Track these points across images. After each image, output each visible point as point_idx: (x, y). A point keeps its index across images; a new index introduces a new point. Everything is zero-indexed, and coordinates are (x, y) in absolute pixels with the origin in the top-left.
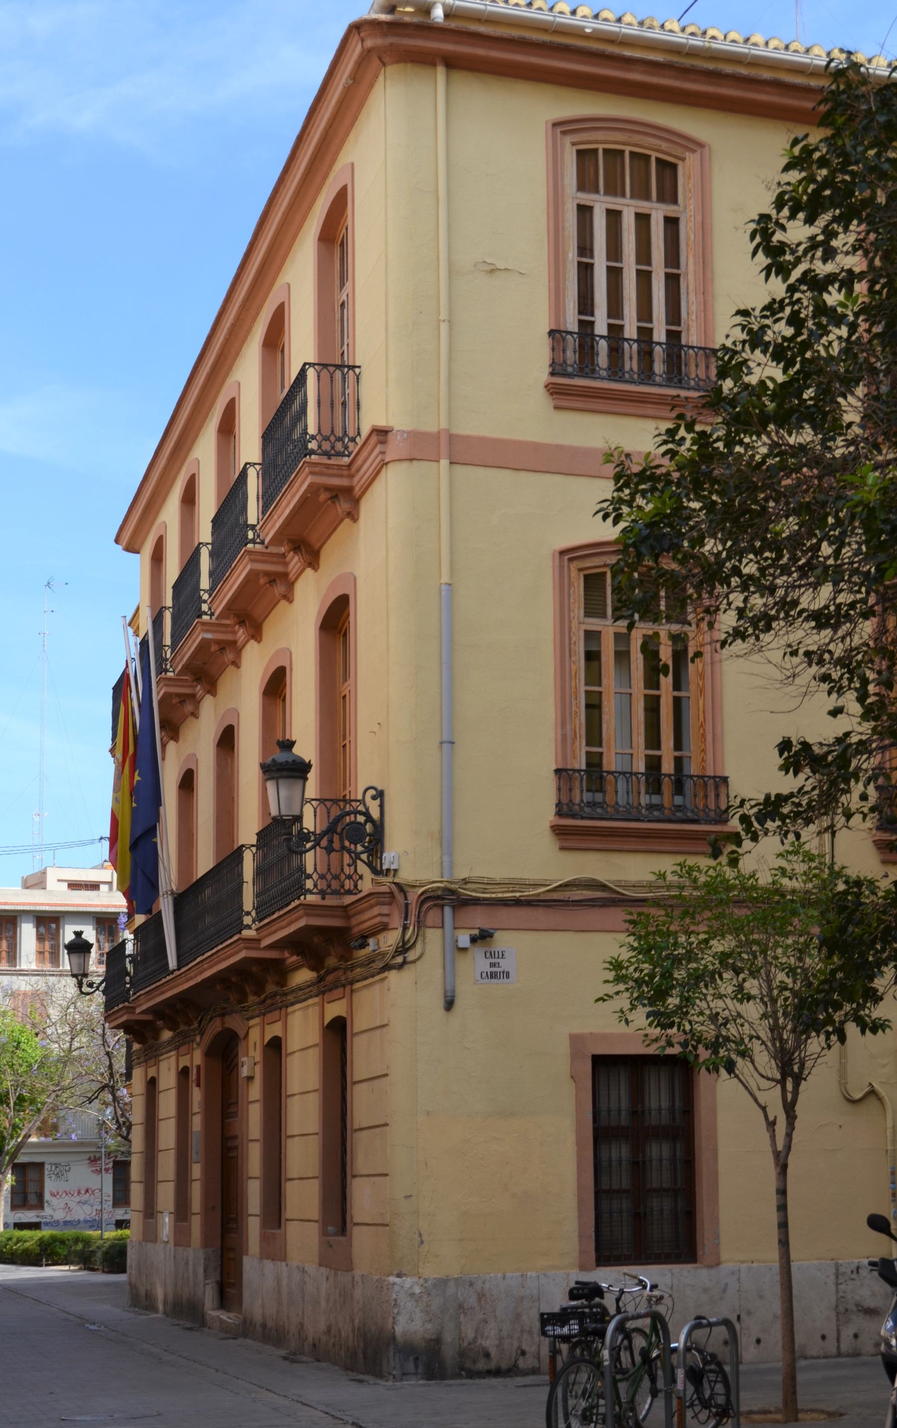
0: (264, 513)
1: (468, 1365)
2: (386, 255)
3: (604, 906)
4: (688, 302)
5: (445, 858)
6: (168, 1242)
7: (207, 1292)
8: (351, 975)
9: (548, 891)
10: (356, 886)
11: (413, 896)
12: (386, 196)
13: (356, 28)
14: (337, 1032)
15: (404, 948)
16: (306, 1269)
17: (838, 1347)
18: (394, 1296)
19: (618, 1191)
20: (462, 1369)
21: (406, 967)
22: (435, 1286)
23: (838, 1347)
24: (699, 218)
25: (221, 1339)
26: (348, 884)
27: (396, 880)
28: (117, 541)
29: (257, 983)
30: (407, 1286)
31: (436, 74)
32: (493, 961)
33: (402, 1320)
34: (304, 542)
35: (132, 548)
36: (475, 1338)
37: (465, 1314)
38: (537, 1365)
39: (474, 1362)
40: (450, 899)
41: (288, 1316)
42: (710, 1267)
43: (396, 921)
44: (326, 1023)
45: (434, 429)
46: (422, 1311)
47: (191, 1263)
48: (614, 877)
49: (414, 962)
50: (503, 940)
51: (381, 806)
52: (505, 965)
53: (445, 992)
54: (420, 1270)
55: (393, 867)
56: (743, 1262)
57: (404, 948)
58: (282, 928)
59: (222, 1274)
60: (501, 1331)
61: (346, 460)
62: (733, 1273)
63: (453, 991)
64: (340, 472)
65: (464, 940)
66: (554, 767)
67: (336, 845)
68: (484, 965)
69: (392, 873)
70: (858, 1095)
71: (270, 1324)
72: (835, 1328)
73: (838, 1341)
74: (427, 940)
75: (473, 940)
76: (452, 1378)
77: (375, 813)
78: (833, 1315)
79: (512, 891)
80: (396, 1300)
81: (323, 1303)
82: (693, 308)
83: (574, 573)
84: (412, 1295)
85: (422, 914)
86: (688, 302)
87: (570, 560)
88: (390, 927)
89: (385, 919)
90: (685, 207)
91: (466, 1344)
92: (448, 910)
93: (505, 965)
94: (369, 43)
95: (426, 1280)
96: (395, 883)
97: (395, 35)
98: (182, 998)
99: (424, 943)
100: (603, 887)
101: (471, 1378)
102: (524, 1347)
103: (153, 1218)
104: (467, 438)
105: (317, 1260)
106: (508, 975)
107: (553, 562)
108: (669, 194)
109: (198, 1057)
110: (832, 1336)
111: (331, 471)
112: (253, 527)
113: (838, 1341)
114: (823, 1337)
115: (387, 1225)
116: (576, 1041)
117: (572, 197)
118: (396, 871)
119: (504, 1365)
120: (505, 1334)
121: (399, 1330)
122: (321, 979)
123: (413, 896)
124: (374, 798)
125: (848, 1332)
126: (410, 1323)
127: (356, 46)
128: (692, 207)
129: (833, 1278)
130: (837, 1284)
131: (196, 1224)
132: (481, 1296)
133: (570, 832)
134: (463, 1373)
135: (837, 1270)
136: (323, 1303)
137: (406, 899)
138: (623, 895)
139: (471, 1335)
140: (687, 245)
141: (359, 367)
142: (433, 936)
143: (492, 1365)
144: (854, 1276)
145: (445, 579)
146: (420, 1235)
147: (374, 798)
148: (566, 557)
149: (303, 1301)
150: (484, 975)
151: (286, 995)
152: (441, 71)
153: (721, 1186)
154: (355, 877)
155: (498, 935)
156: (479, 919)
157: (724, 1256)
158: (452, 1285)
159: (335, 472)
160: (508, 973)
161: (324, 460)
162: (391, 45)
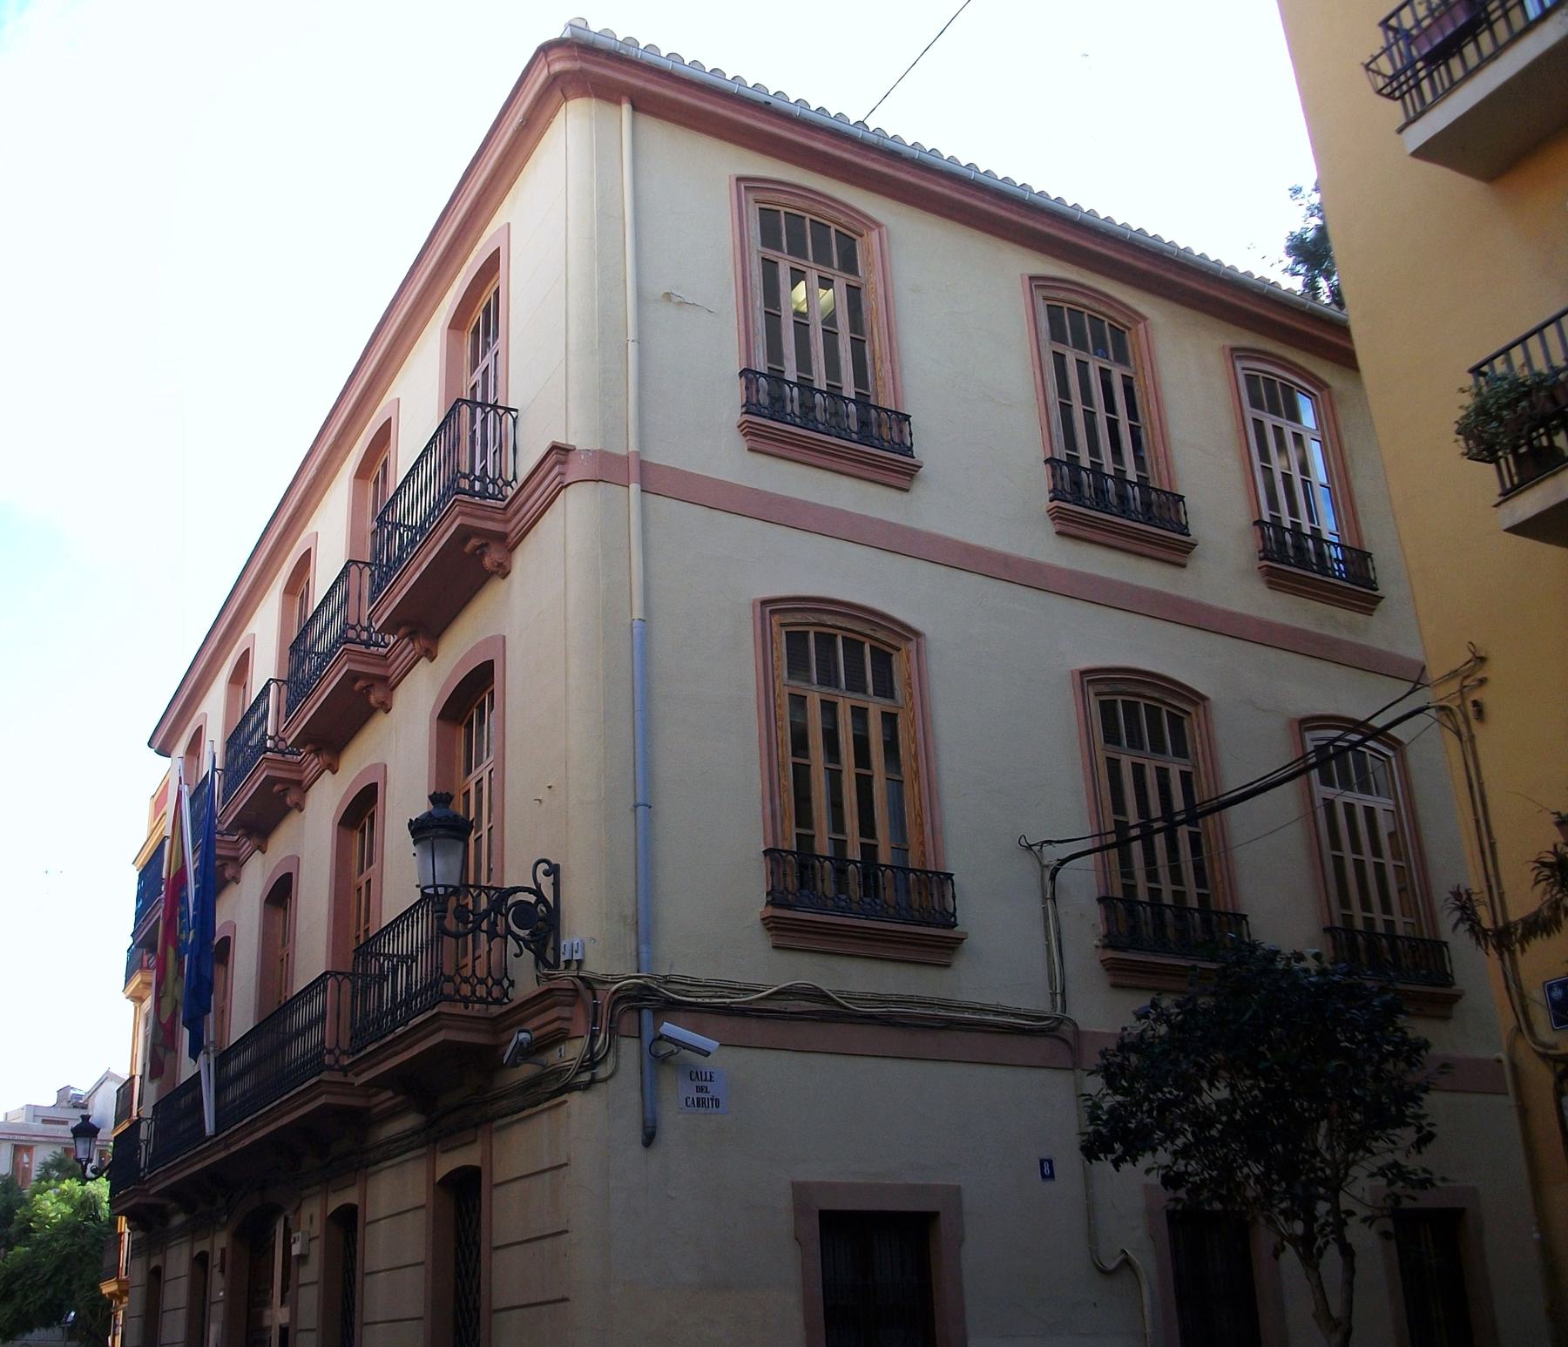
3: (822, 1020)
5: (643, 948)
11: (603, 998)
13: (545, 49)
14: (463, 1194)
15: (591, 1061)
26: (496, 992)
27: (582, 974)
28: (150, 744)
29: (332, 1146)
32: (701, 1084)
34: (427, 616)
35: (164, 751)
40: (646, 999)
43: (580, 1025)
49: (605, 1080)
51: (556, 885)
53: (644, 1122)
57: (591, 1061)
58: (396, 1054)
63: (655, 1120)
67: (500, 929)
69: (574, 966)
70: (1112, 1266)
74: (621, 1054)
77: (548, 893)
87: (772, 612)
89: (565, 1025)
93: (714, 1089)
94: (557, 67)
97: (585, 60)
98: (212, 1173)
99: (617, 1057)
100: (822, 996)
109: (222, 1240)
116: (799, 1189)
118: (580, 962)
124: (546, 874)
133: (783, 929)
145: (636, 616)
147: (546, 874)
152: (626, 109)
154: (506, 983)
161: (279, 757)
162: (581, 70)
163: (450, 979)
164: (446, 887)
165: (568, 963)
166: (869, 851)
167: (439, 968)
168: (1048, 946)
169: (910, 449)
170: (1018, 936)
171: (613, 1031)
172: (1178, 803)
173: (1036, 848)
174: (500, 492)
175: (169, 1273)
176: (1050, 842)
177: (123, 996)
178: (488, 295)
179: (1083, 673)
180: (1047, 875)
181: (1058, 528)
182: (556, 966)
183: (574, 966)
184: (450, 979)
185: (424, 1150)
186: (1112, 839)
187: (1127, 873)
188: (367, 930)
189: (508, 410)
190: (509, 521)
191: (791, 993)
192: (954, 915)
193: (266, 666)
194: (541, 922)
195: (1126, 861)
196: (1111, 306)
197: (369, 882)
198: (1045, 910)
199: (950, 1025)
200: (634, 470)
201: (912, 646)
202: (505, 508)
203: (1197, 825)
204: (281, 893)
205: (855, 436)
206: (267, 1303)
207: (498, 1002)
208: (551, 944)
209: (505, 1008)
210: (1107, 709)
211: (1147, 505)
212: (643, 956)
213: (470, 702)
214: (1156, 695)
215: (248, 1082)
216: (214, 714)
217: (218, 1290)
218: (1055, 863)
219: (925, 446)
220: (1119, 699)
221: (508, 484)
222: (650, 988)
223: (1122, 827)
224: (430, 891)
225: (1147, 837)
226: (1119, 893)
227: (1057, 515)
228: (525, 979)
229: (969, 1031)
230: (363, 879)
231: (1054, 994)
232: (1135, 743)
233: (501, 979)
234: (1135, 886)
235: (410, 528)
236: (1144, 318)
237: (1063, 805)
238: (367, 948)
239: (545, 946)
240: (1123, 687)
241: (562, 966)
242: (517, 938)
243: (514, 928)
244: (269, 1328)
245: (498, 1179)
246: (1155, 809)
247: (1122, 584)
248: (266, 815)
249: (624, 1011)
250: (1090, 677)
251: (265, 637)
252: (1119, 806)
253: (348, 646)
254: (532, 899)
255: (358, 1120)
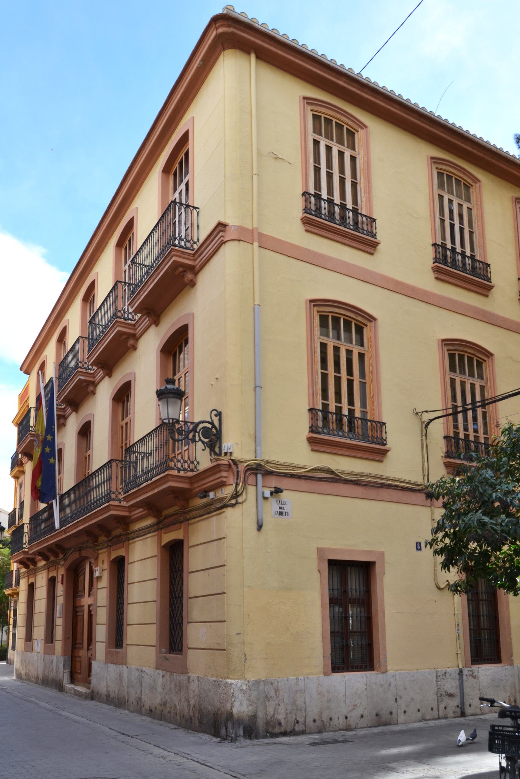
0: (58, 392)
1: (270, 730)
2: (224, 140)
3: (331, 482)
4: (361, 196)
6: (39, 652)
7: (65, 676)
8: (188, 516)
9: (306, 471)
10: (196, 467)
11: (242, 468)
12: (225, 112)
15: (236, 495)
16: (144, 670)
17: (439, 714)
18: (232, 691)
19: (355, 632)
20: (267, 732)
21: (236, 506)
22: (253, 685)
23: (439, 714)
24: (366, 159)
25: (172, 729)
27: (232, 458)
28: (21, 369)
29: (114, 532)
30: (239, 685)
31: (250, 56)
33: (237, 705)
34: (153, 309)
36: (274, 714)
37: (269, 701)
38: (304, 729)
39: (273, 728)
40: (258, 469)
41: (128, 693)
42: (383, 673)
43: (231, 480)
44: (163, 544)
45: (250, 228)
46: (247, 699)
47: (54, 662)
48: (337, 468)
49: (242, 503)
50: (285, 496)
52: (286, 508)
54: (245, 676)
55: (229, 451)
56: (397, 670)
57: (236, 495)
59: (71, 668)
60: (286, 710)
61: (92, 372)
62: (393, 677)
64: (189, 257)
65: (267, 494)
66: (308, 408)
67: (197, 439)
68: (276, 507)
69: (229, 454)
71: (112, 695)
72: (437, 704)
73: (438, 711)
75: (272, 493)
76: (262, 738)
77: (216, 424)
78: (435, 697)
79: (289, 470)
80: (233, 693)
81: (159, 689)
82: (364, 199)
83: (315, 313)
84: (242, 690)
85: (246, 477)
86: (361, 196)
88: (227, 484)
89: (224, 479)
90: (359, 153)
91: (269, 718)
92: (259, 476)
94: (220, 30)
95: (249, 682)
96: (232, 460)
97: (234, 28)
100: (332, 472)
101: (272, 737)
102: (298, 719)
103: (31, 641)
104: (266, 235)
105: (154, 666)
106: (287, 514)
107: (306, 305)
108: (352, 147)
109: (62, 571)
110: (435, 708)
111: (184, 256)
112: (32, 427)
113: (438, 711)
114: (432, 709)
115: (225, 650)
116: (320, 551)
117: (311, 136)
118: (231, 453)
119: (288, 730)
120: (288, 711)
121: (235, 711)
122: (158, 523)
123: (242, 468)
125: (442, 706)
126: (241, 707)
127: (212, 32)
128: (362, 154)
129: (435, 678)
130: (437, 681)
131: (59, 646)
132: (277, 690)
133: (315, 443)
134: (268, 734)
135: (437, 674)
136: (159, 689)
137: (238, 468)
138: (340, 477)
139: (272, 713)
140: (360, 170)
141: (198, 208)
142: (251, 489)
143: (282, 730)
144: (444, 677)
146: (245, 656)
147: (216, 415)
148: (312, 304)
149: (141, 686)
150: (276, 513)
151: (129, 534)
152: (253, 56)
153: (386, 630)
154: (195, 463)
155: (284, 491)
156: (274, 482)
157: (389, 668)
158: (262, 684)
159: (186, 256)
160: (288, 513)
161: (84, 370)
163: (114, 493)
164: (173, 419)
165: (226, 454)
166: (351, 412)
167: (110, 489)
168: (423, 456)
169: (375, 235)
170: (413, 452)
171: (245, 482)
172: (478, 398)
173: (420, 414)
174: (192, 246)
175: (37, 585)
176: (427, 411)
177: (10, 476)
178: (182, 155)
179: (443, 340)
180: (424, 426)
181: (436, 275)
182: (220, 454)
183: (229, 454)
184: (114, 493)
185: (156, 533)
186: (450, 411)
187: (456, 427)
188: (126, 444)
189: (195, 208)
190: (195, 260)
191: (319, 470)
192: (385, 440)
193: (74, 333)
194: (213, 436)
195: (456, 420)
196: (465, 174)
197: (126, 424)
198: (422, 440)
199: (383, 486)
200: (256, 236)
201: (373, 324)
202: (194, 254)
203: (485, 409)
204: (85, 431)
205: (352, 227)
206: (83, 596)
207: (192, 470)
208: (218, 446)
209: (194, 473)
210: (452, 357)
211: (474, 268)
212: (258, 452)
213: (176, 345)
214: (472, 352)
215: (71, 509)
216: (50, 354)
217: (60, 589)
218: (428, 421)
219: (382, 233)
220: (457, 353)
221: (195, 243)
222: (260, 465)
223: (455, 407)
224: (166, 421)
225: (465, 411)
226: (452, 435)
227: (436, 270)
228: (204, 459)
229: (390, 489)
230: (124, 422)
231: (424, 475)
232: (462, 371)
233: (194, 462)
234: (459, 433)
235: (146, 266)
236: (479, 181)
237: (434, 397)
238: (129, 450)
239: (215, 446)
240: (458, 348)
241: (223, 454)
242: (203, 443)
243: (202, 438)
244: (83, 606)
245: (191, 544)
246: (469, 400)
247: (461, 303)
248: (78, 396)
249: (250, 474)
250: (446, 342)
251: (74, 322)
252: (454, 398)
253: (118, 319)
254: (210, 426)
255: (124, 522)
